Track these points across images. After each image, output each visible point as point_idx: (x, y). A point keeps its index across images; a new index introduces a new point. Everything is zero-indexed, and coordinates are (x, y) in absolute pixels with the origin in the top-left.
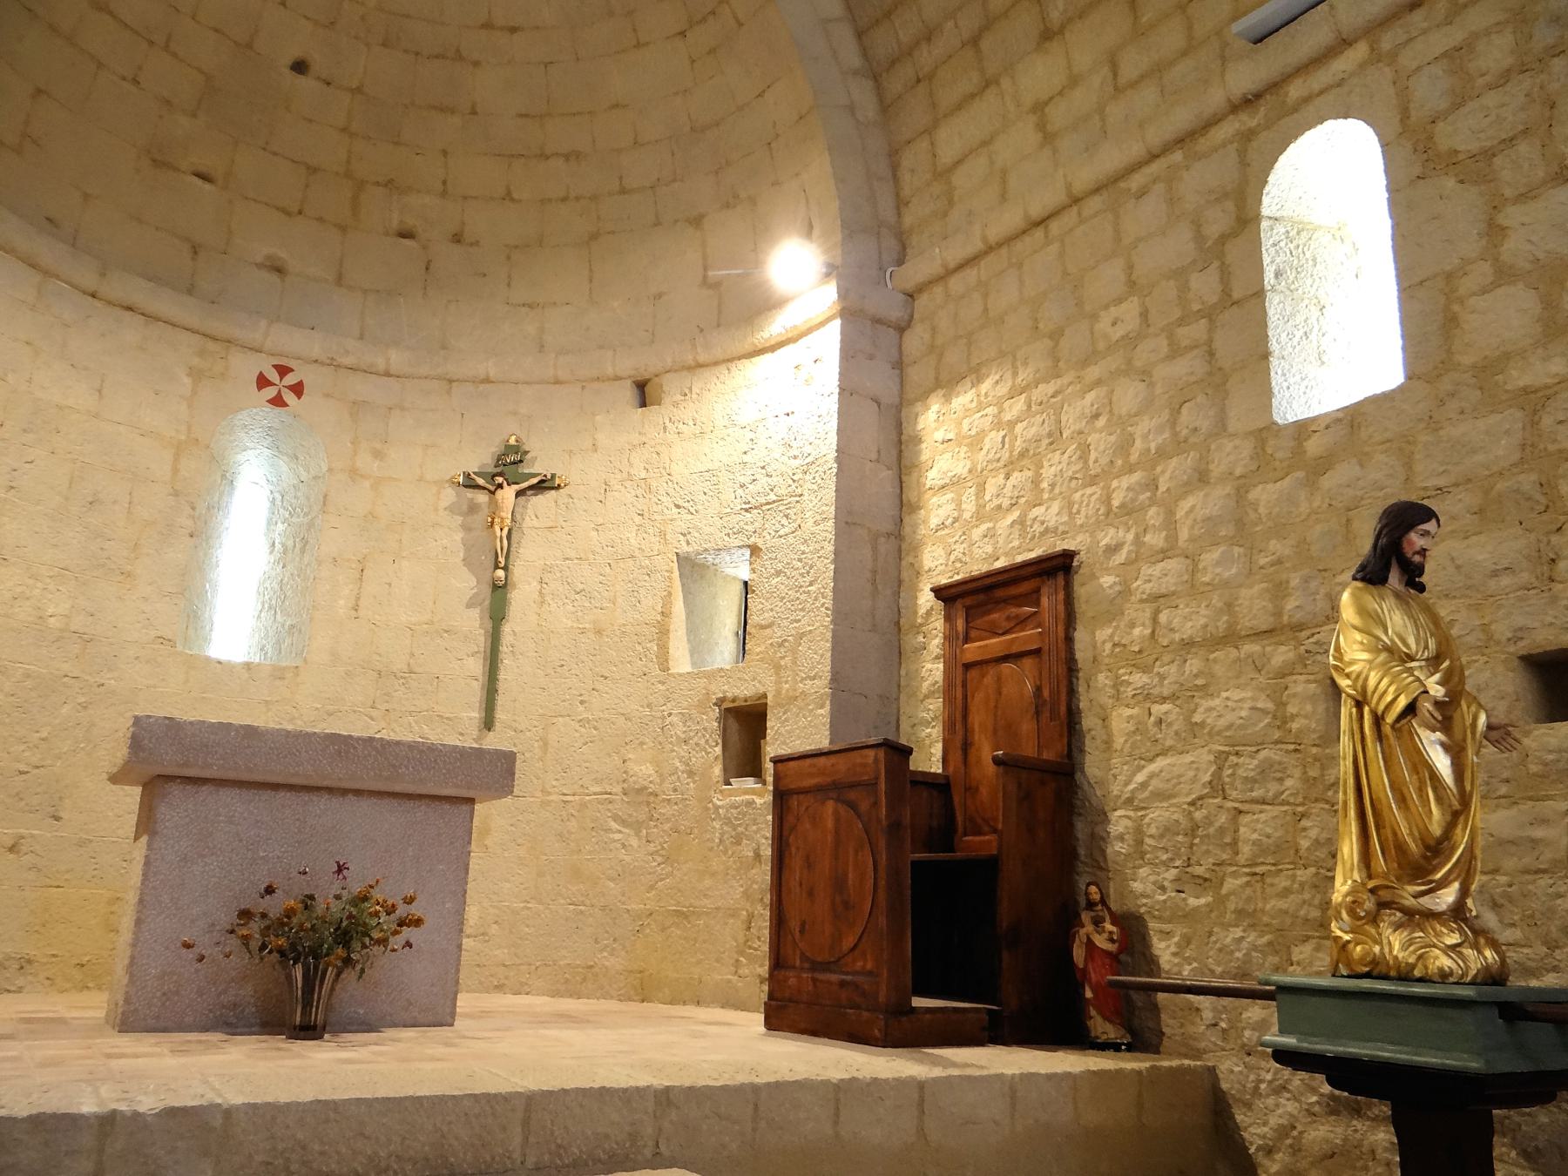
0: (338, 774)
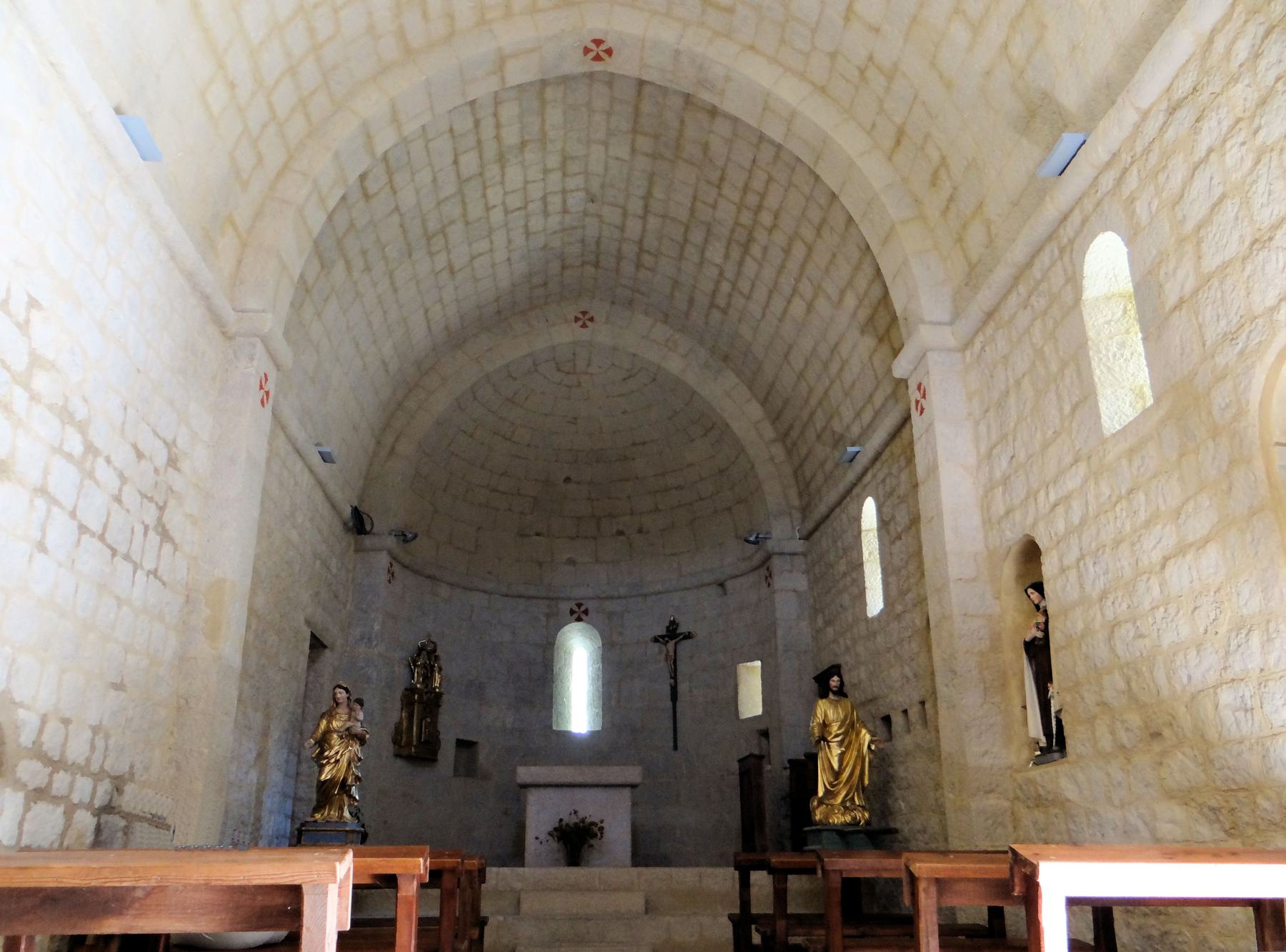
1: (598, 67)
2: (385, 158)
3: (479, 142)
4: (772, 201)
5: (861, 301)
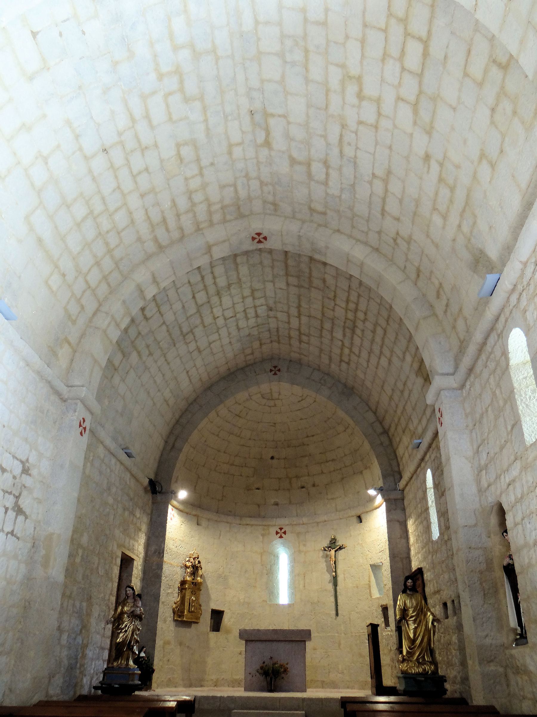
0: (275, 637)
1: (261, 246)
2: (154, 298)
3: (205, 286)
4: (362, 306)
5: (414, 358)
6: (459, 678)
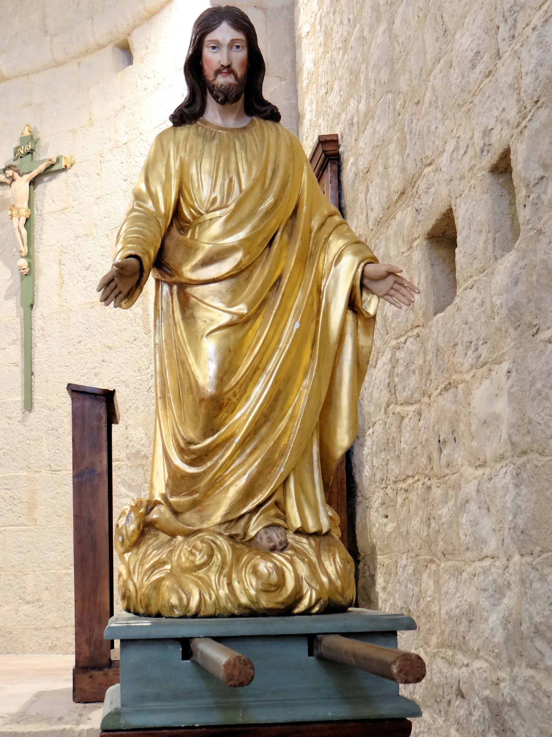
6: (494, 619)
